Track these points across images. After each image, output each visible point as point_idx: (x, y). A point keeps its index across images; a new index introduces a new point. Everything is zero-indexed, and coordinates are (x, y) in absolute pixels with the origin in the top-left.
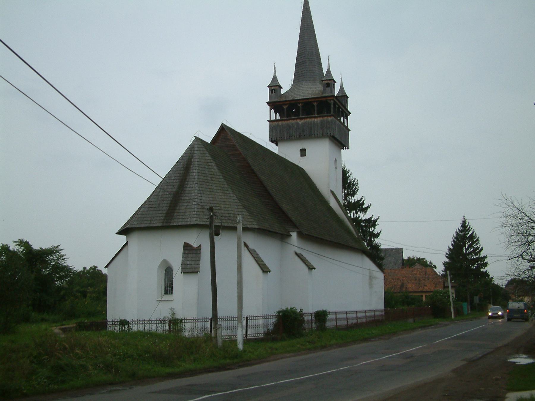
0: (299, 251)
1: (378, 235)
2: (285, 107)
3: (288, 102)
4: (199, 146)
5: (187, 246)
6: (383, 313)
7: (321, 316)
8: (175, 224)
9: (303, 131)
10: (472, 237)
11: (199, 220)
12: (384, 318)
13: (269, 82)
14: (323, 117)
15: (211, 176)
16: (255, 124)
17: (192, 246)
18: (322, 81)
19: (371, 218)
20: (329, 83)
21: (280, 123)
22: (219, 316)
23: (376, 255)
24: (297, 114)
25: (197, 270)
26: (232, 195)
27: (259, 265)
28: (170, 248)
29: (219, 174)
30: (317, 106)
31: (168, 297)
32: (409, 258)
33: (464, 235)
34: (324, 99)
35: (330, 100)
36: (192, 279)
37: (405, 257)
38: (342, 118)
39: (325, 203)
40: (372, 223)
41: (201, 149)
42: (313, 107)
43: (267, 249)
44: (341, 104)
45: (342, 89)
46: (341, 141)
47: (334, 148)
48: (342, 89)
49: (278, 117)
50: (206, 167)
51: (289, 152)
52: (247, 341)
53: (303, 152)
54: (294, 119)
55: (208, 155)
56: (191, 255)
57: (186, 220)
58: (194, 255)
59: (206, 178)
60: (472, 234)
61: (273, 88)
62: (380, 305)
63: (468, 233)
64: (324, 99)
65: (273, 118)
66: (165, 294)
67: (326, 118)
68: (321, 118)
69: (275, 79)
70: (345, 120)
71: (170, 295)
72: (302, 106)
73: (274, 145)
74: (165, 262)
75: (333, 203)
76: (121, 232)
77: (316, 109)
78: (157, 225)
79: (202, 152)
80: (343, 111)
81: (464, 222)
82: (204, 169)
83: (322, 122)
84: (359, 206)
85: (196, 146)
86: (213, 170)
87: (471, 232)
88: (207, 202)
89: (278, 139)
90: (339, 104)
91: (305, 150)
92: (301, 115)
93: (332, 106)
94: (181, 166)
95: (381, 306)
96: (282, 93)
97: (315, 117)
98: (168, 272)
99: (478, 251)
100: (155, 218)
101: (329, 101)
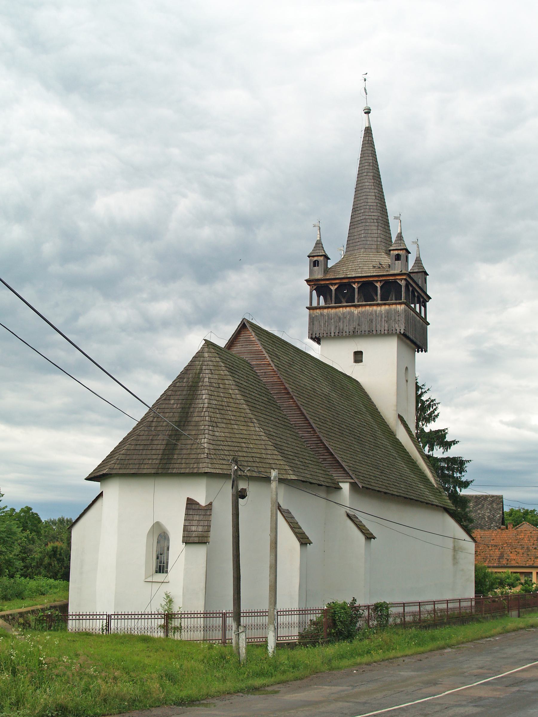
0: (351, 513)
2: (333, 288)
4: (211, 355)
5: (191, 503)
6: (473, 603)
7: (380, 609)
8: (175, 471)
9: (359, 325)
11: (210, 466)
12: (473, 610)
13: (310, 248)
14: (389, 304)
15: (228, 400)
17: (198, 504)
18: (390, 250)
20: (402, 255)
21: (326, 311)
23: (460, 511)
24: (350, 300)
25: (205, 540)
26: (257, 429)
27: (295, 533)
28: (167, 503)
29: (239, 397)
30: (381, 287)
31: (160, 577)
32: (512, 510)
35: (401, 280)
36: (200, 553)
37: (506, 509)
38: (418, 305)
40: (458, 464)
41: (213, 359)
43: (307, 508)
44: (417, 285)
45: (418, 261)
46: (415, 339)
47: (406, 351)
48: (418, 261)
49: (322, 303)
50: (221, 386)
51: (336, 355)
52: (279, 646)
53: (358, 356)
54: (346, 307)
55: (224, 368)
56: (197, 518)
57: (191, 466)
59: (220, 403)
61: (315, 258)
65: (315, 304)
67: (394, 306)
68: (387, 307)
69: (319, 244)
70: (423, 308)
71: (165, 574)
72: (359, 288)
73: (315, 344)
74: (157, 525)
75: (402, 436)
76: (90, 478)
77: (379, 292)
79: (215, 364)
80: (419, 296)
82: (217, 390)
83: (388, 312)
84: (439, 438)
85: (206, 355)
86: (231, 391)
88: (223, 439)
89: (321, 336)
90: (414, 285)
91: (361, 353)
92: (356, 300)
95: (471, 593)
97: (378, 305)
98: (161, 537)
100: (146, 461)
101: (399, 281)
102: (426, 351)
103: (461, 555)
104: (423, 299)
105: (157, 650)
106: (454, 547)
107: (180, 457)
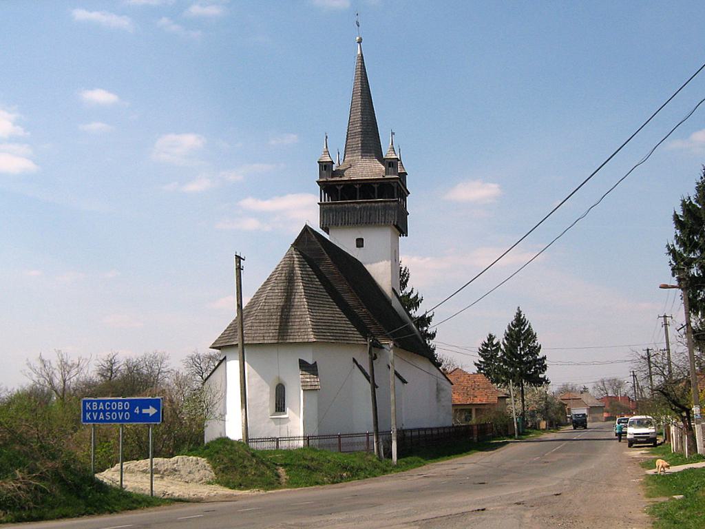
1: (432, 336)
2: (339, 188)
3: (343, 183)
8: (291, 341)
10: (529, 332)
17: (307, 363)
19: (425, 315)
21: (333, 206)
22: (379, 431)
33: (520, 330)
34: (388, 181)
53: (360, 243)
60: (528, 329)
63: (524, 329)
64: (388, 181)
66: (276, 411)
72: (360, 188)
78: (272, 341)
81: (519, 314)
87: (527, 326)
93: (396, 190)
94: (283, 278)
99: (536, 350)
102: (407, 236)
103: (443, 394)
104: (403, 194)
105: (571, 515)
106: (437, 388)
107: (293, 331)
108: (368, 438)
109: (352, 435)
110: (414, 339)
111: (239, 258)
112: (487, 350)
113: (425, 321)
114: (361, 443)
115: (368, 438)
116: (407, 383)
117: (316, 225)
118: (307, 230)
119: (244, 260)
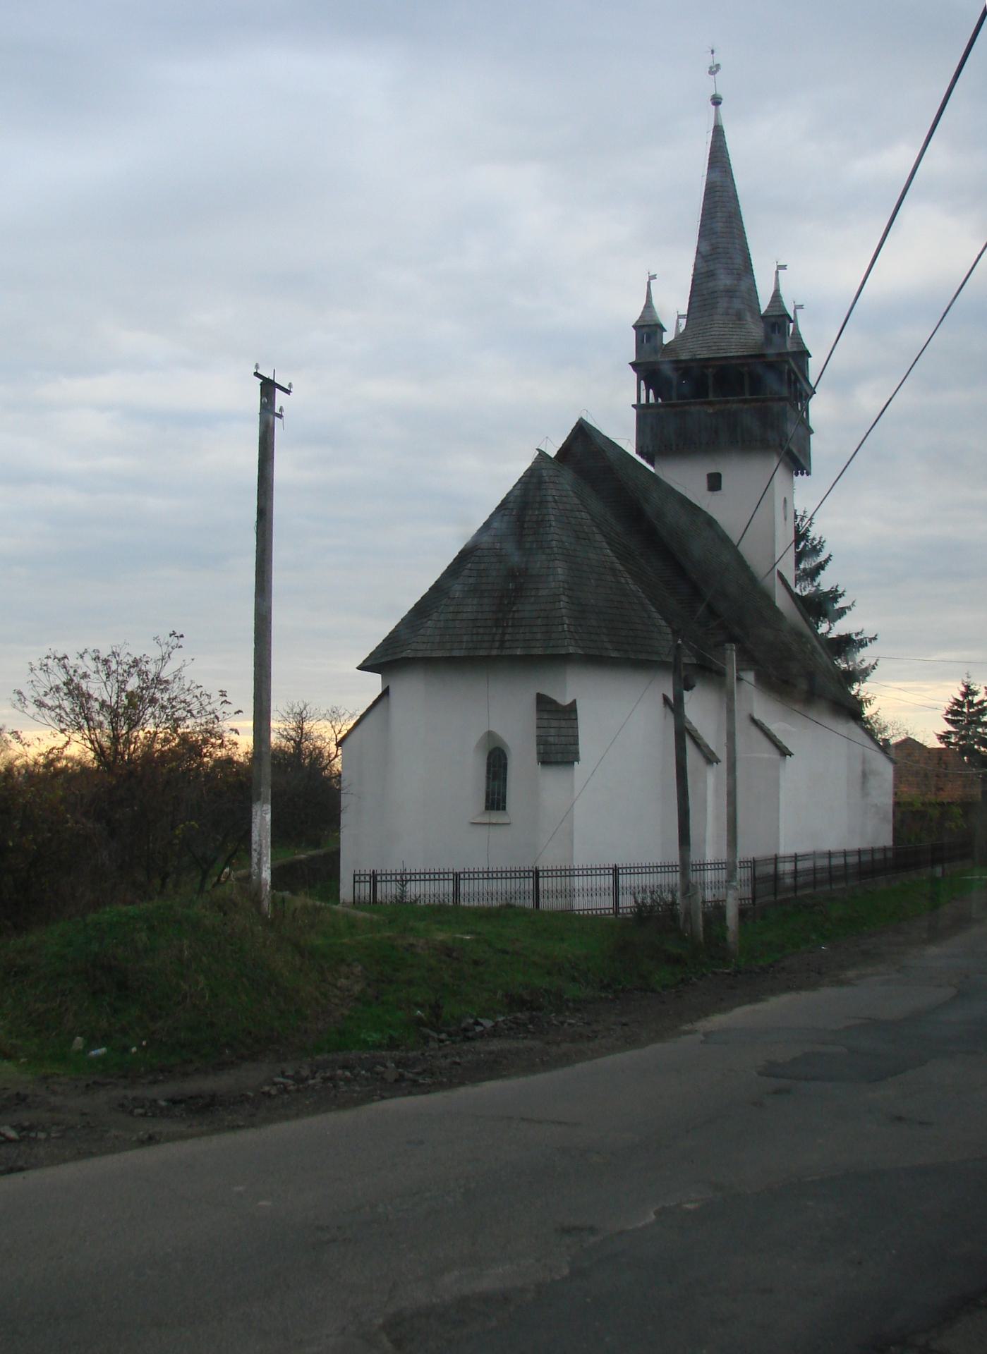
16: (618, 415)
31: (496, 817)
39: (768, 598)
42: (731, 378)
49: (652, 400)
53: (714, 482)
58: (563, 723)
61: (645, 330)
62: (883, 837)
74: (490, 735)
75: (782, 601)
96: (665, 342)
98: (497, 763)
102: (808, 474)
108: (616, 881)
109: (569, 873)
110: (819, 675)
111: (268, 387)
112: (961, 713)
113: (846, 644)
114: (599, 892)
115: (616, 881)
116: (790, 754)
117: (626, 439)
118: (583, 433)
119: (288, 392)
